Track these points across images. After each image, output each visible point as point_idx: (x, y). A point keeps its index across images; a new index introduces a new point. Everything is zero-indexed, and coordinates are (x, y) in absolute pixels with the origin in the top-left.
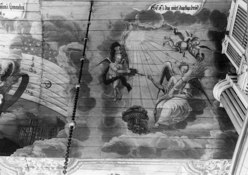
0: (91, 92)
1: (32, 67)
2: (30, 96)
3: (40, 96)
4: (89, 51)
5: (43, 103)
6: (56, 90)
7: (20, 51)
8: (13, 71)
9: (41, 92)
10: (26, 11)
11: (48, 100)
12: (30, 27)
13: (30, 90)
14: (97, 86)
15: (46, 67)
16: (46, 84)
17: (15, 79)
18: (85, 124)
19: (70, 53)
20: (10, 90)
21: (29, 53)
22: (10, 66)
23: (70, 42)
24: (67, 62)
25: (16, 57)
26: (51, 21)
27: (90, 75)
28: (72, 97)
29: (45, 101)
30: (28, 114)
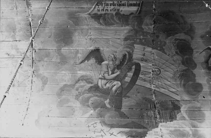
22: (125, 56)
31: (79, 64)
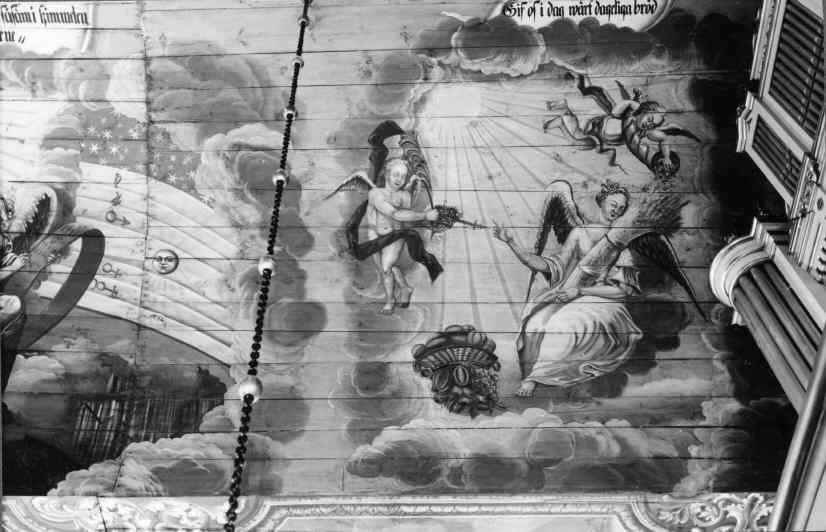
0: (309, 284)
5: (154, 323)
6: (193, 279)
7: (76, 156)
8: (51, 220)
9: (147, 285)
11: (170, 311)
12: (108, 77)
13: (110, 282)
14: (330, 264)
16: (160, 259)
17: (58, 246)
18: (293, 387)
19: (237, 160)
21: (103, 161)
22: (44, 204)
24: (229, 190)
25: (60, 174)
28: (247, 299)
30: (103, 357)
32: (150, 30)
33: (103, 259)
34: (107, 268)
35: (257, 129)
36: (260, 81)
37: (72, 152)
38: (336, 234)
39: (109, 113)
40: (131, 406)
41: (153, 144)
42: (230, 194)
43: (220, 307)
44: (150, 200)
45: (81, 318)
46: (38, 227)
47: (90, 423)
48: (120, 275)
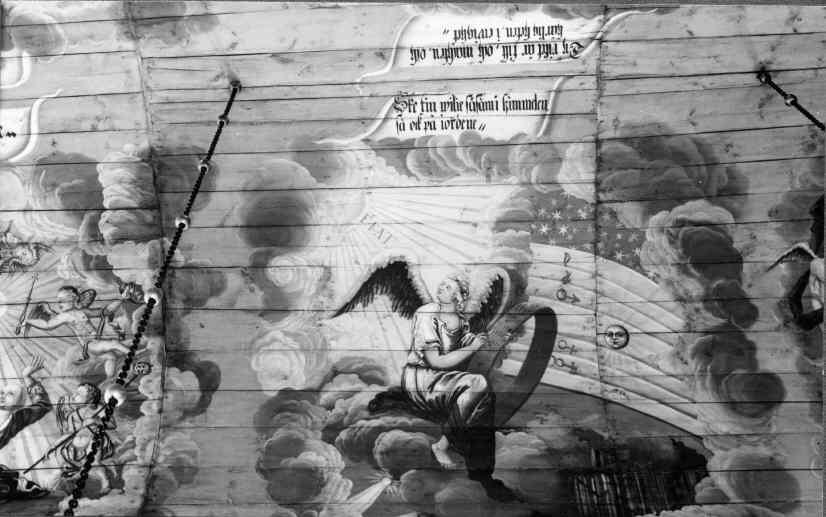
0: (760, 355)
1: (565, 283)
2: (568, 375)
3: (602, 374)
4: (743, 226)
5: (617, 397)
6: (646, 353)
7: (527, 237)
8: (505, 300)
9: (603, 361)
10: (552, 115)
11: (627, 384)
12: (560, 160)
13: (568, 358)
14: (776, 334)
15: (610, 283)
16: (611, 334)
17: (512, 325)
18: (772, 459)
19: (680, 236)
20: (504, 361)
21: (552, 241)
22: (497, 285)
23: (681, 200)
24: (672, 265)
25: (510, 255)
26: (625, 140)
27: (745, 299)
28: (701, 371)
29: (620, 389)
30: (576, 431)
31: (335, 316)
32: (605, 115)
33: (558, 336)
34: (563, 344)
35: (700, 206)
36: (706, 159)
37: (524, 233)
38: (779, 304)
39: (559, 194)
40: (621, 480)
41: (601, 224)
42: (674, 270)
43: (675, 380)
44: (598, 278)
45: (546, 394)
46: (492, 307)
47: (588, 498)
48: (576, 351)
